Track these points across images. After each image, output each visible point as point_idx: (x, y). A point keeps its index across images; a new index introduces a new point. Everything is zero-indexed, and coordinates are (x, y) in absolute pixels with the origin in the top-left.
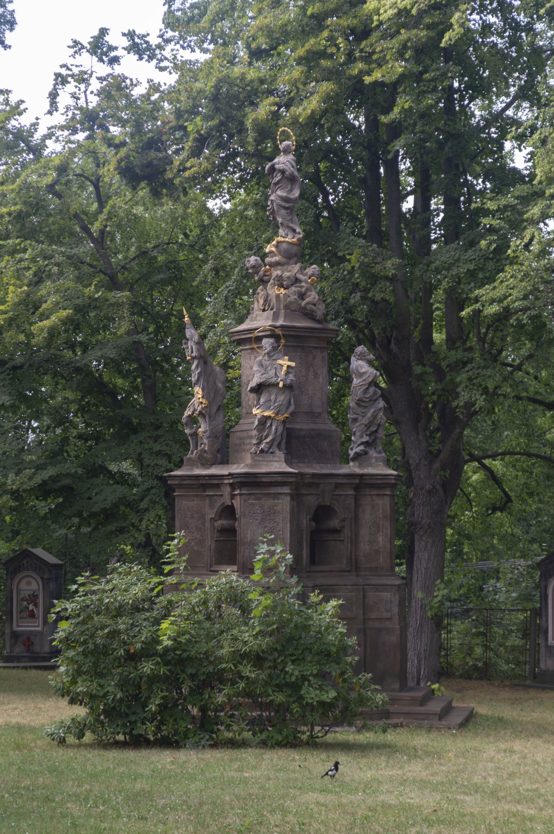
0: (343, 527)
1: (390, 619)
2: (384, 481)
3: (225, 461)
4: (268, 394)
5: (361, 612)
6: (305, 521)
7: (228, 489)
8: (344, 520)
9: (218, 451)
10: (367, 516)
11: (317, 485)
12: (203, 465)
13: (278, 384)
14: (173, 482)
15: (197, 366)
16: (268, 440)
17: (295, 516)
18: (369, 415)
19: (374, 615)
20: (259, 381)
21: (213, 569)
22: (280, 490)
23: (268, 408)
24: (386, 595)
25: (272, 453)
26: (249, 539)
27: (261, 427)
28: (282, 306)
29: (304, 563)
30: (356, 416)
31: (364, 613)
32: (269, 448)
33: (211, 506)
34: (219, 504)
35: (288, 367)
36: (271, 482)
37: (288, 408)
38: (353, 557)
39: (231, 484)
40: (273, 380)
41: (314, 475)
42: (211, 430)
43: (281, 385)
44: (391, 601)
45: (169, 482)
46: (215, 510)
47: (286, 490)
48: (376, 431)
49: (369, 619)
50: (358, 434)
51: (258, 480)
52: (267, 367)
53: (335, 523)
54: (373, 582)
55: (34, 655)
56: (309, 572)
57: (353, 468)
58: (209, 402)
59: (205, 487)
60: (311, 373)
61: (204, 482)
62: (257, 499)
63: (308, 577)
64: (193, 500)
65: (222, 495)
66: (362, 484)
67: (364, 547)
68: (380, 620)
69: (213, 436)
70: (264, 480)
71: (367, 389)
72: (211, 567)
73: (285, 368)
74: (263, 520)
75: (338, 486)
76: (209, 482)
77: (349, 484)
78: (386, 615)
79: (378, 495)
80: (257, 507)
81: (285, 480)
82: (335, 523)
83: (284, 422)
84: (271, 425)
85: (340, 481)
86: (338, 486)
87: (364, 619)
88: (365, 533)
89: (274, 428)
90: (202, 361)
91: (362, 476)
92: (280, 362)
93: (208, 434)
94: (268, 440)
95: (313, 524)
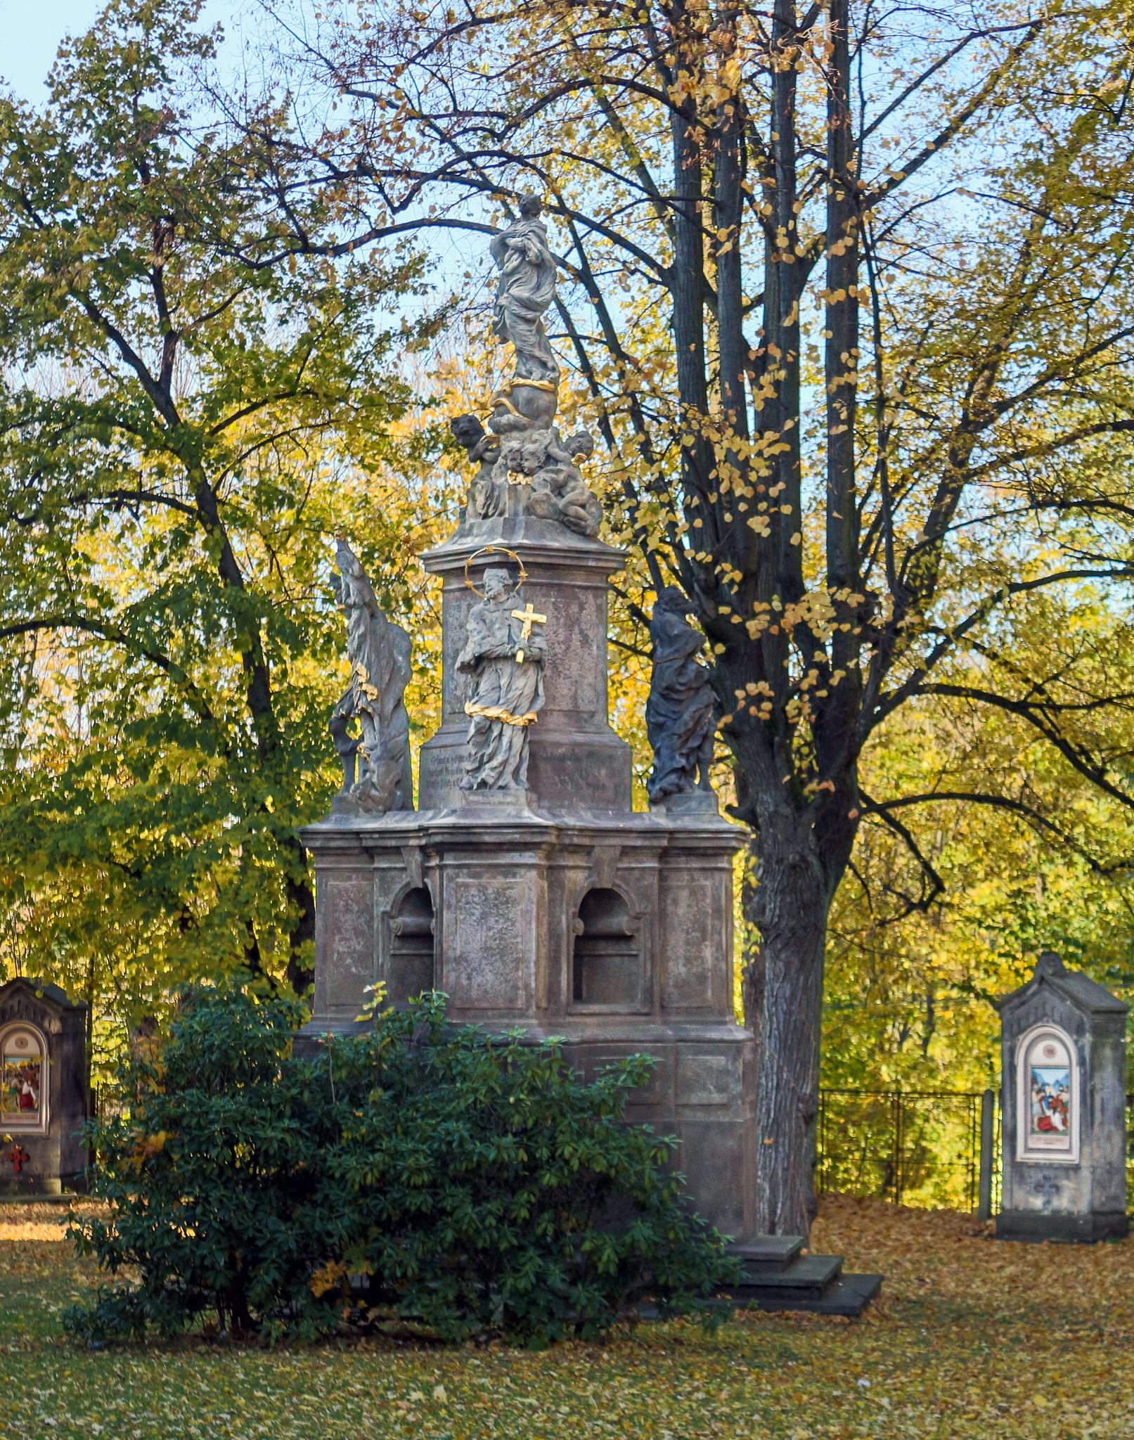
0: (638, 930)
6: (568, 922)
7: (418, 857)
13: (514, 656)
16: (495, 763)
17: (550, 906)
20: (479, 651)
22: (516, 858)
23: (497, 703)
24: (719, 1061)
25: (501, 788)
30: (661, 719)
37: (532, 702)
39: (422, 849)
40: (506, 649)
46: (392, 897)
47: (528, 858)
49: (685, 1106)
51: (475, 839)
52: (493, 623)
53: (620, 922)
59: (370, 853)
60: (576, 637)
61: (370, 843)
64: (350, 878)
65: (404, 869)
67: (678, 969)
68: (707, 1107)
70: (487, 839)
73: (527, 626)
74: (484, 916)
75: (626, 851)
76: (381, 843)
78: (717, 1098)
80: (473, 891)
81: (528, 839)
84: (501, 734)
86: (626, 851)
89: (505, 740)
90: (367, 613)
91: (671, 832)
92: (517, 613)
95: (580, 926)
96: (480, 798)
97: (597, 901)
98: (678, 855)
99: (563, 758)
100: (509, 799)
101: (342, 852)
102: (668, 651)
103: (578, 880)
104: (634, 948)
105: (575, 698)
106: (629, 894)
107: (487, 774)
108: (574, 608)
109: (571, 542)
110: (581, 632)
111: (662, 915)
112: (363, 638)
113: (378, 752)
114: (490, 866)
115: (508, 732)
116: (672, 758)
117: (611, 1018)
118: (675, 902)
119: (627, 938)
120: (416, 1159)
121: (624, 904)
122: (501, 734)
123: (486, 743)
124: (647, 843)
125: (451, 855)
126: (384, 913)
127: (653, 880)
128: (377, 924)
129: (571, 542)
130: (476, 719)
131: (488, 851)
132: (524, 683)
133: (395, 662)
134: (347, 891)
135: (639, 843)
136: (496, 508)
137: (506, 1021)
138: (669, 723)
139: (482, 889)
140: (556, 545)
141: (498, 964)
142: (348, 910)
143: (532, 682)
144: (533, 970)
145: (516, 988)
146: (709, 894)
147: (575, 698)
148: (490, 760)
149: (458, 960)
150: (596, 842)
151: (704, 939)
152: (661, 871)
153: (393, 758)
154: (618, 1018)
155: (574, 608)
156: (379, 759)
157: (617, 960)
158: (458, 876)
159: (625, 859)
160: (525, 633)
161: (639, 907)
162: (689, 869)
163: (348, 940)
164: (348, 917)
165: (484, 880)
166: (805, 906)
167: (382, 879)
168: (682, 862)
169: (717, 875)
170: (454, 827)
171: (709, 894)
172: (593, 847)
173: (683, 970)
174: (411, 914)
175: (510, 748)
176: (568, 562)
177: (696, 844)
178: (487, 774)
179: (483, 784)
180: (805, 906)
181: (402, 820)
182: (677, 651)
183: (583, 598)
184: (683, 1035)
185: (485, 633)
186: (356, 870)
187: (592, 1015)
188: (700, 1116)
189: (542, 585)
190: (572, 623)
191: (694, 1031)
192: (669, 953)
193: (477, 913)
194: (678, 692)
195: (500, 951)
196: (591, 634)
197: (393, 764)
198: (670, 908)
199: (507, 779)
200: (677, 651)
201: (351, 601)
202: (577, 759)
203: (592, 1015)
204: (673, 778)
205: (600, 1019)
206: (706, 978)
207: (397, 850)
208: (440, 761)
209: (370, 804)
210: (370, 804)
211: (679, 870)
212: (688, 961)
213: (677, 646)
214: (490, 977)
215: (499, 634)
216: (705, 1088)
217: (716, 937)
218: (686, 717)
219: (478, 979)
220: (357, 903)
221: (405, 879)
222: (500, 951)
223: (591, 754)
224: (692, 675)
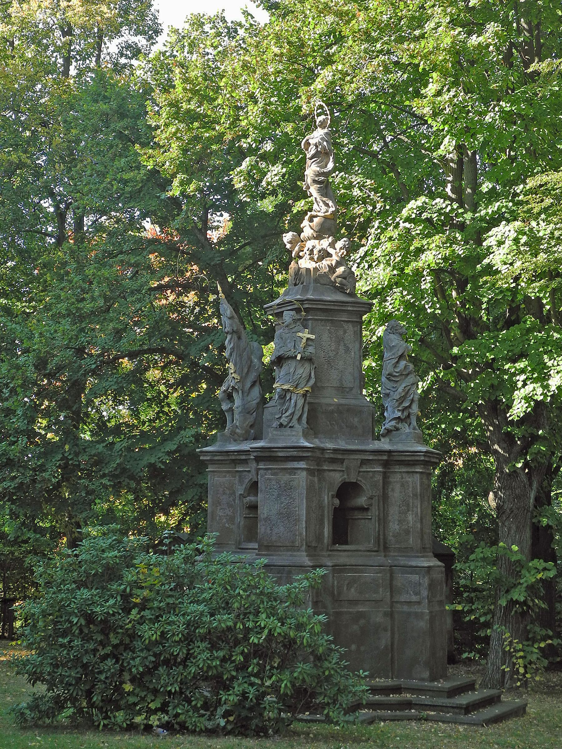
0: (371, 505)
1: (419, 603)
2: (413, 458)
3: (256, 438)
4: (287, 367)
5: (388, 594)
6: (328, 499)
8: (371, 498)
9: (252, 426)
10: (396, 494)
11: (342, 461)
12: (235, 440)
13: (296, 356)
14: (205, 458)
15: (230, 342)
16: (287, 414)
17: (312, 492)
18: (400, 390)
19: (403, 598)
22: (296, 465)
23: (288, 382)
24: (415, 578)
25: (290, 427)
26: (266, 515)
27: (282, 401)
28: (312, 281)
29: (326, 541)
30: (388, 391)
31: (392, 596)
34: (247, 480)
37: (308, 381)
38: (381, 537)
40: (291, 354)
41: (335, 451)
42: (244, 405)
43: (299, 358)
44: (420, 584)
45: (201, 458)
46: (244, 486)
47: (302, 465)
48: (410, 407)
49: (397, 602)
52: (286, 340)
53: (362, 501)
54: (402, 563)
55: (11, 635)
56: (331, 551)
57: (384, 445)
58: (241, 378)
59: (235, 462)
60: (342, 348)
61: (233, 458)
63: (329, 556)
64: (225, 476)
65: (249, 471)
66: (390, 460)
67: (394, 526)
68: (409, 603)
69: (246, 411)
70: (280, 454)
71: (397, 362)
73: (304, 340)
74: (279, 496)
75: (364, 462)
76: (238, 457)
77: (375, 460)
78: (414, 598)
80: (274, 482)
81: (301, 454)
82: (362, 501)
83: (305, 395)
84: (290, 399)
86: (364, 462)
87: (392, 602)
88: (394, 511)
89: (293, 401)
90: (235, 336)
91: (390, 452)
92: (300, 334)
93: (240, 409)
94: (287, 414)
95: (337, 502)
97: (346, 490)
99: (332, 412)
100: (293, 433)
104: (369, 515)
105: (341, 380)
106: (365, 485)
107: (284, 420)
108: (341, 332)
109: (340, 297)
110: (345, 345)
112: (233, 348)
116: (394, 412)
117: (356, 553)
118: (393, 490)
119: (367, 509)
120: (177, 625)
121: (364, 491)
123: (284, 403)
126: (241, 494)
127: (379, 478)
129: (340, 297)
130: (278, 390)
131: (281, 461)
132: (303, 371)
133: (251, 362)
136: (300, 280)
137: (290, 553)
138: (392, 393)
139: (278, 482)
140: (329, 299)
141: (286, 522)
144: (304, 526)
145: (295, 535)
146: (411, 486)
147: (341, 380)
150: (345, 457)
151: (409, 511)
152: (385, 473)
153: (248, 413)
154: (360, 553)
155: (341, 332)
156: (240, 413)
157: (363, 521)
158: (266, 475)
159: (364, 466)
160: (302, 345)
162: (401, 472)
163: (224, 509)
164: (224, 496)
166: (518, 497)
167: (240, 477)
168: (397, 469)
170: (262, 448)
171: (411, 486)
173: (397, 527)
176: (336, 308)
179: (281, 425)
180: (518, 497)
182: (394, 354)
183: (346, 327)
184: (396, 563)
185: (281, 345)
187: (345, 551)
188: (406, 608)
189: (322, 320)
190: (339, 340)
191: (403, 561)
192: (390, 518)
194: (395, 376)
195: (287, 515)
196: (350, 346)
197: (248, 416)
198: (390, 494)
199: (294, 422)
200: (394, 354)
203: (345, 551)
204: (393, 423)
205: (350, 553)
206: (409, 532)
207: (245, 462)
210: (236, 437)
211: (395, 472)
214: (282, 529)
215: (289, 345)
216: (407, 592)
217: (415, 509)
218: (400, 390)
219: (276, 530)
222: (287, 515)
224: (403, 367)
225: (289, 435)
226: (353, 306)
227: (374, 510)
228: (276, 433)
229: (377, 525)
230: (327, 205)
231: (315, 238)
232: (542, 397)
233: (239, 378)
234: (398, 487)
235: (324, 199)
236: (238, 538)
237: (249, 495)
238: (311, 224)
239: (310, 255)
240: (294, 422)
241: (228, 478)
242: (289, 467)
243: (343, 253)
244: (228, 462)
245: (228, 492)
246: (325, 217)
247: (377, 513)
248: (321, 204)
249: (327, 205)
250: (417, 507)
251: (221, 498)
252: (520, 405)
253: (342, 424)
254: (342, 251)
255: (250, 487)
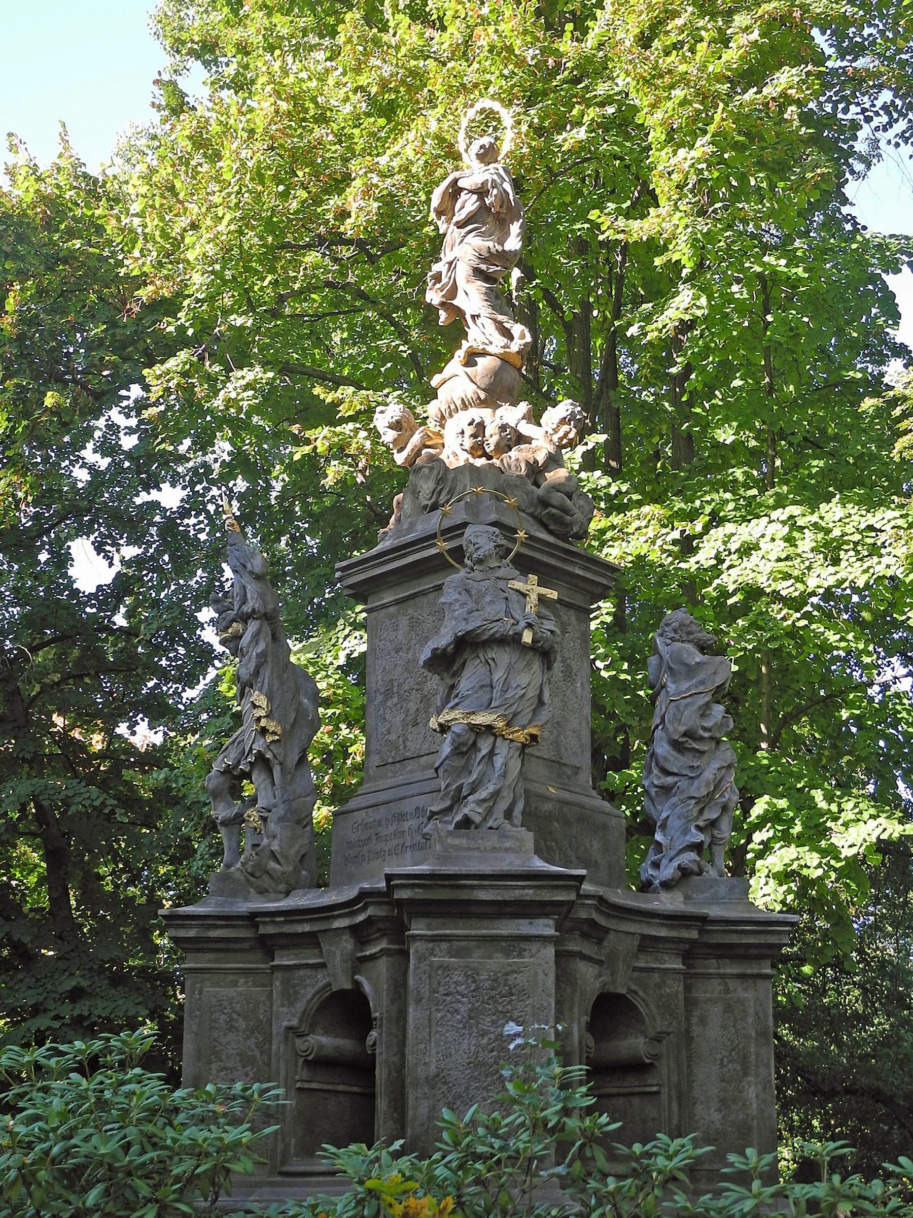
0: (657, 1057)
7: (347, 944)
8: (658, 1039)
13: (519, 635)
15: (256, 636)
16: (483, 794)
20: (463, 628)
21: (286, 1168)
22: (524, 927)
23: (488, 707)
26: (433, 1069)
32: (485, 819)
33: (290, 998)
34: (311, 991)
35: (541, 599)
36: (505, 903)
39: (354, 930)
40: (505, 627)
46: (300, 1007)
47: (545, 927)
50: (675, 824)
51: (464, 895)
58: (283, 730)
59: (267, 946)
61: (270, 930)
62: (458, 954)
64: (235, 984)
65: (323, 966)
70: (483, 895)
72: (284, 1162)
74: (474, 1015)
75: (648, 944)
76: (287, 929)
79: (742, 977)
80: (458, 977)
81: (546, 896)
84: (492, 754)
85: (654, 932)
86: (648, 944)
89: (499, 761)
94: (483, 794)
96: (464, 842)
98: (707, 957)
100: (507, 845)
101: (224, 946)
102: (685, 685)
103: (590, 978)
106: (647, 1004)
107: (470, 808)
111: (688, 1037)
113: (280, 811)
114: (484, 939)
115: (502, 749)
118: (703, 1021)
121: (642, 1021)
122: (492, 754)
123: (466, 769)
124: (674, 934)
125: (423, 922)
127: (675, 987)
128: (276, 1045)
131: (481, 916)
132: (528, 678)
133: (300, 704)
134: (231, 1001)
135: (663, 933)
139: (472, 974)
142: (231, 1028)
143: (537, 682)
146: (751, 1011)
148: (473, 791)
149: (433, 1082)
151: (746, 1074)
156: (281, 819)
158: (432, 953)
159: (643, 957)
161: (661, 1024)
162: (722, 976)
164: (231, 1036)
165: (474, 960)
167: (286, 982)
168: (711, 966)
169: (760, 982)
171: (751, 1011)
172: (607, 930)
173: (716, 1116)
174: (326, 1032)
175: (504, 775)
177: (735, 939)
178: (470, 808)
179: (466, 823)
181: (320, 897)
185: (471, 605)
186: (244, 972)
192: (696, 1092)
193: (463, 1009)
194: (702, 738)
198: (696, 1030)
200: (702, 683)
201: (247, 608)
202: (567, 823)
206: (750, 1128)
207: (312, 940)
208: (367, 826)
209: (266, 882)
210: (266, 882)
211: (709, 976)
212: (724, 1103)
213: (701, 677)
217: (762, 1070)
220: (246, 1018)
221: (321, 979)
223: (581, 819)
225: (494, 849)
226: (586, 569)
227: (665, 1071)
228: (457, 841)
229: (675, 1108)
230: (507, 334)
231: (483, 403)
232: (820, 872)
233: (279, 730)
234: (716, 1012)
235: (500, 318)
236: (280, 1147)
237: (312, 1031)
238: (469, 370)
239: (474, 436)
240: (497, 819)
241: (244, 987)
242: (504, 932)
243: (566, 434)
244: (246, 945)
245: (242, 1025)
246: (504, 359)
247: (675, 1078)
248: (491, 328)
249: (507, 334)
250: (767, 1066)
251: (224, 1040)
252: (767, 890)
253: (570, 853)
254: (565, 428)
255: (319, 1009)
